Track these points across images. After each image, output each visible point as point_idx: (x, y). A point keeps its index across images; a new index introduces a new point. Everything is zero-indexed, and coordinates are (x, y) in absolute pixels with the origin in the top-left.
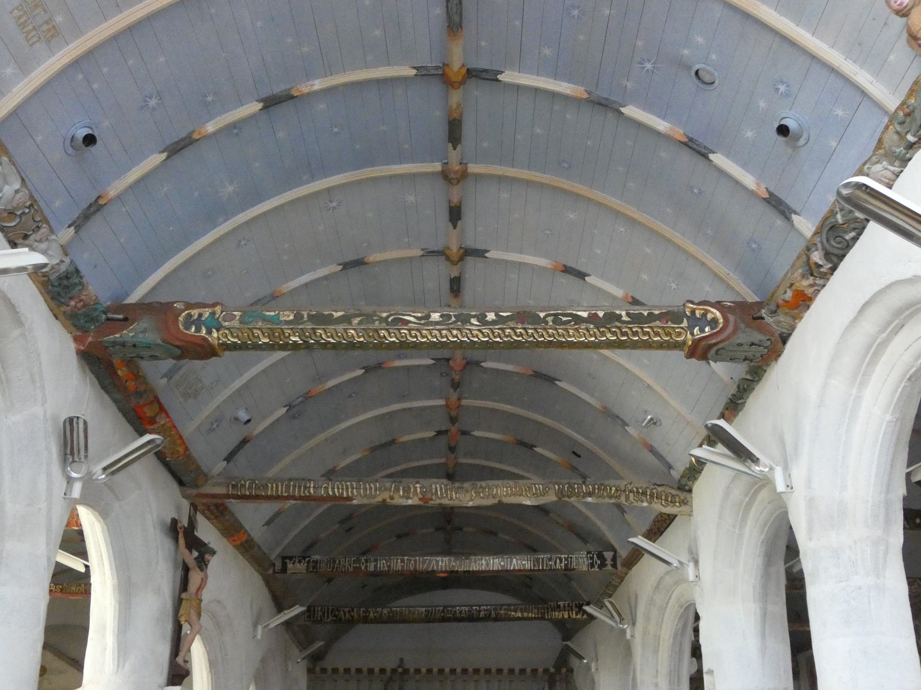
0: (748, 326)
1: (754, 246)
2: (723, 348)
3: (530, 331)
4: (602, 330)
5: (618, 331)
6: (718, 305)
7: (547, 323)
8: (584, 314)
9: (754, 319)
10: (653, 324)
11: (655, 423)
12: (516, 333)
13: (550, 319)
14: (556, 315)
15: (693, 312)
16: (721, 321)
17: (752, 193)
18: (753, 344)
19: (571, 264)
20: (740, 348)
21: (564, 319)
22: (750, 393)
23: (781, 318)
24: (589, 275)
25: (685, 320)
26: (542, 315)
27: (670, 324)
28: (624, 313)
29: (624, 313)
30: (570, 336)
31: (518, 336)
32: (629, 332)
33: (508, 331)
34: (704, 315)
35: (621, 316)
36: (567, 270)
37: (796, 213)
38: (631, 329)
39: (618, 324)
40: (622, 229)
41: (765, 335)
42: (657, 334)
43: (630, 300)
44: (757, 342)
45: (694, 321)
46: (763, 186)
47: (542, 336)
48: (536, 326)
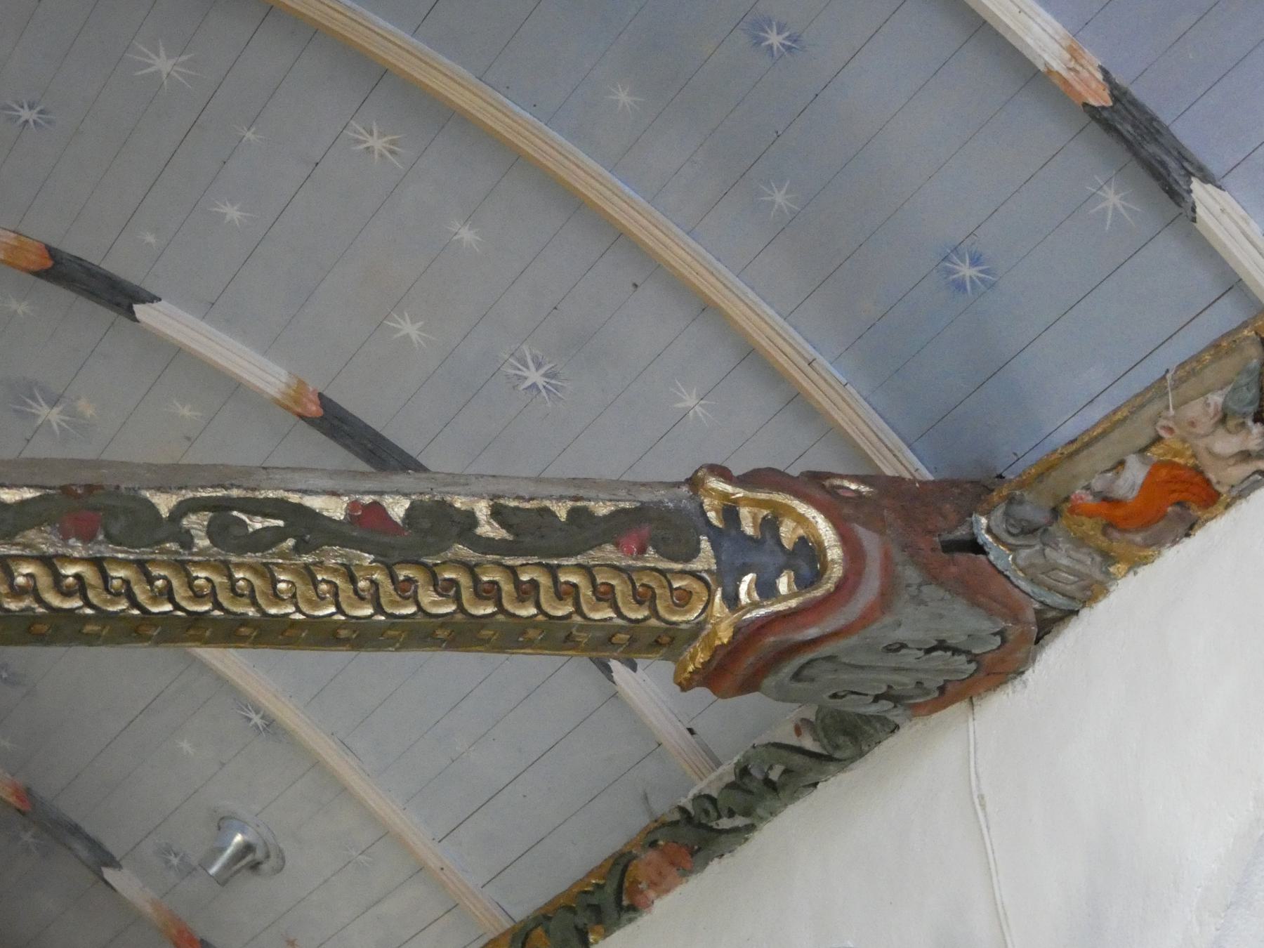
0: (933, 577)
1: (967, 271)
2: (830, 658)
3: (118, 573)
4: (402, 574)
5: (464, 580)
6: (814, 486)
7: (186, 540)
8: (335, 509)
9: (951, 547)
10: (593, 557)
11: (255, 866)
12: (58, 579)
13: (196, 523)
14: (219, 507)
15: (730, 512)
16: (834, 553)
17: (1033, 78)
18: (942, 646)
19: (77, 245)
20: (892, 660)
21: (257, 524)
22: (794, 798)
23: (1062, 555)
24: (153, 299)
25: (705, 544)
26: (164, 503)
27: (652, 558)
28: (482, 509)
29: (482, 509)
30: (277, 597)
31: (67, 594)
32: (507, 587)
33: (27, 569)
34: (770, 526)
35: (470, 519)
36: (62, 270)
37: (1207, 178)
38: (513, 571)
39: (462, 551)
40: (378, 143)
41: (991, 613)
42: (605, 595)
43: (314, 409)
44: (957, 639)
45: (742, 551)
46: (1092, 62)
47: (168, 594)
48: (106, 551)
